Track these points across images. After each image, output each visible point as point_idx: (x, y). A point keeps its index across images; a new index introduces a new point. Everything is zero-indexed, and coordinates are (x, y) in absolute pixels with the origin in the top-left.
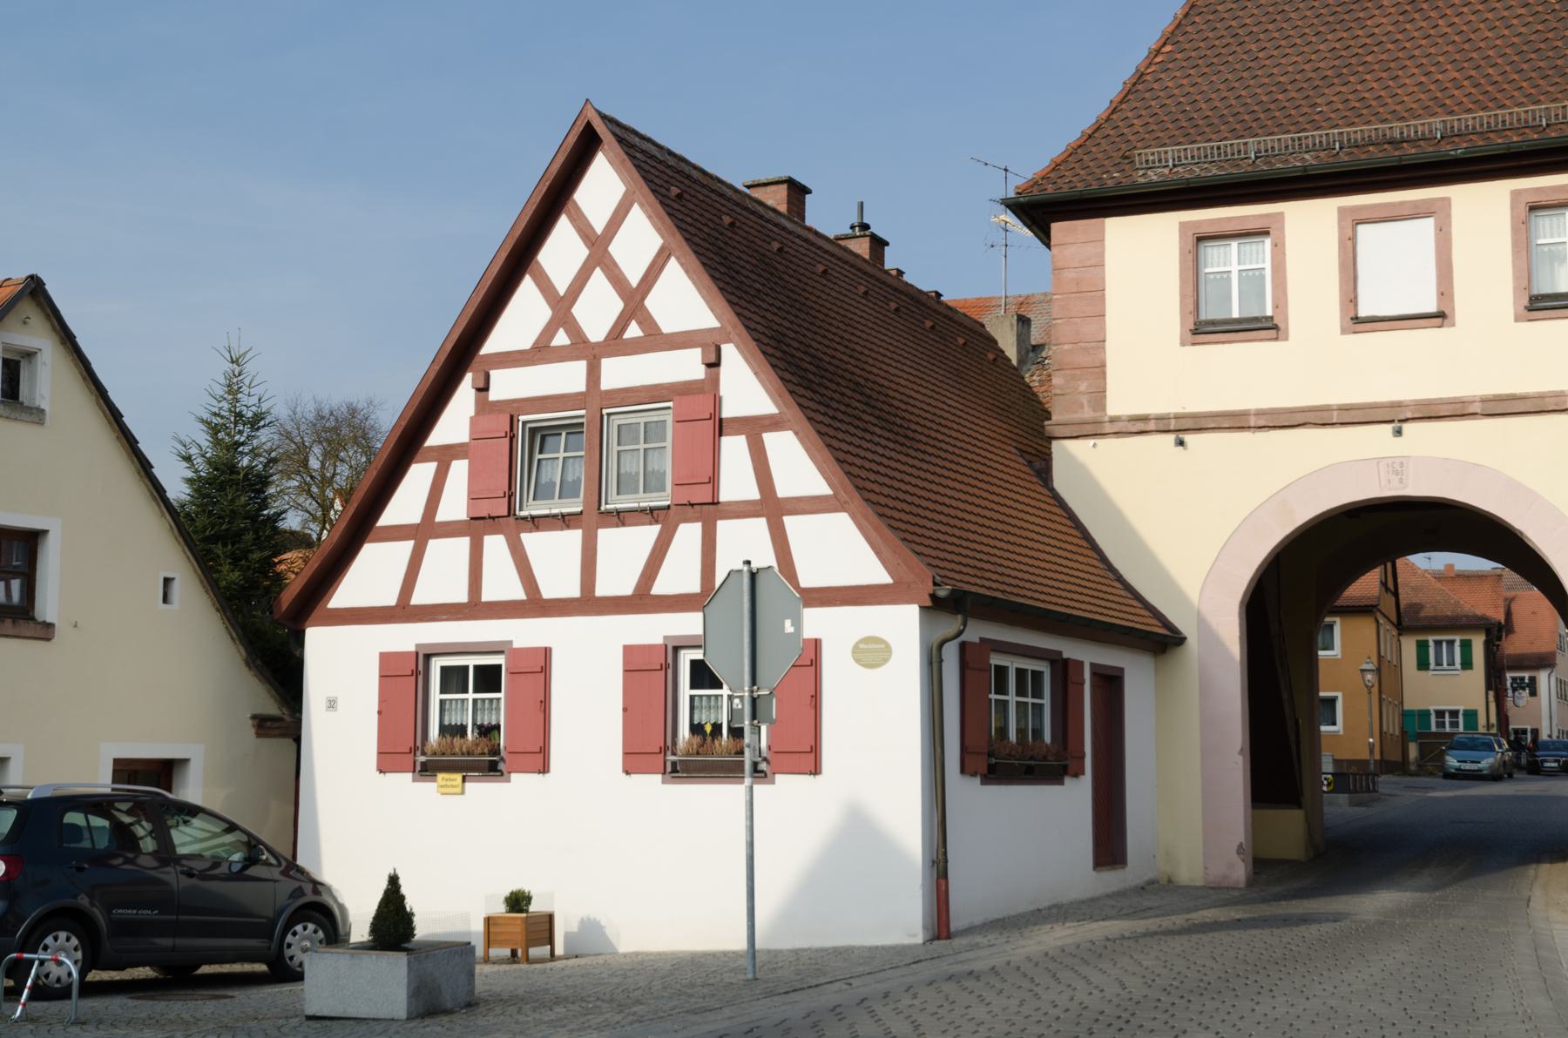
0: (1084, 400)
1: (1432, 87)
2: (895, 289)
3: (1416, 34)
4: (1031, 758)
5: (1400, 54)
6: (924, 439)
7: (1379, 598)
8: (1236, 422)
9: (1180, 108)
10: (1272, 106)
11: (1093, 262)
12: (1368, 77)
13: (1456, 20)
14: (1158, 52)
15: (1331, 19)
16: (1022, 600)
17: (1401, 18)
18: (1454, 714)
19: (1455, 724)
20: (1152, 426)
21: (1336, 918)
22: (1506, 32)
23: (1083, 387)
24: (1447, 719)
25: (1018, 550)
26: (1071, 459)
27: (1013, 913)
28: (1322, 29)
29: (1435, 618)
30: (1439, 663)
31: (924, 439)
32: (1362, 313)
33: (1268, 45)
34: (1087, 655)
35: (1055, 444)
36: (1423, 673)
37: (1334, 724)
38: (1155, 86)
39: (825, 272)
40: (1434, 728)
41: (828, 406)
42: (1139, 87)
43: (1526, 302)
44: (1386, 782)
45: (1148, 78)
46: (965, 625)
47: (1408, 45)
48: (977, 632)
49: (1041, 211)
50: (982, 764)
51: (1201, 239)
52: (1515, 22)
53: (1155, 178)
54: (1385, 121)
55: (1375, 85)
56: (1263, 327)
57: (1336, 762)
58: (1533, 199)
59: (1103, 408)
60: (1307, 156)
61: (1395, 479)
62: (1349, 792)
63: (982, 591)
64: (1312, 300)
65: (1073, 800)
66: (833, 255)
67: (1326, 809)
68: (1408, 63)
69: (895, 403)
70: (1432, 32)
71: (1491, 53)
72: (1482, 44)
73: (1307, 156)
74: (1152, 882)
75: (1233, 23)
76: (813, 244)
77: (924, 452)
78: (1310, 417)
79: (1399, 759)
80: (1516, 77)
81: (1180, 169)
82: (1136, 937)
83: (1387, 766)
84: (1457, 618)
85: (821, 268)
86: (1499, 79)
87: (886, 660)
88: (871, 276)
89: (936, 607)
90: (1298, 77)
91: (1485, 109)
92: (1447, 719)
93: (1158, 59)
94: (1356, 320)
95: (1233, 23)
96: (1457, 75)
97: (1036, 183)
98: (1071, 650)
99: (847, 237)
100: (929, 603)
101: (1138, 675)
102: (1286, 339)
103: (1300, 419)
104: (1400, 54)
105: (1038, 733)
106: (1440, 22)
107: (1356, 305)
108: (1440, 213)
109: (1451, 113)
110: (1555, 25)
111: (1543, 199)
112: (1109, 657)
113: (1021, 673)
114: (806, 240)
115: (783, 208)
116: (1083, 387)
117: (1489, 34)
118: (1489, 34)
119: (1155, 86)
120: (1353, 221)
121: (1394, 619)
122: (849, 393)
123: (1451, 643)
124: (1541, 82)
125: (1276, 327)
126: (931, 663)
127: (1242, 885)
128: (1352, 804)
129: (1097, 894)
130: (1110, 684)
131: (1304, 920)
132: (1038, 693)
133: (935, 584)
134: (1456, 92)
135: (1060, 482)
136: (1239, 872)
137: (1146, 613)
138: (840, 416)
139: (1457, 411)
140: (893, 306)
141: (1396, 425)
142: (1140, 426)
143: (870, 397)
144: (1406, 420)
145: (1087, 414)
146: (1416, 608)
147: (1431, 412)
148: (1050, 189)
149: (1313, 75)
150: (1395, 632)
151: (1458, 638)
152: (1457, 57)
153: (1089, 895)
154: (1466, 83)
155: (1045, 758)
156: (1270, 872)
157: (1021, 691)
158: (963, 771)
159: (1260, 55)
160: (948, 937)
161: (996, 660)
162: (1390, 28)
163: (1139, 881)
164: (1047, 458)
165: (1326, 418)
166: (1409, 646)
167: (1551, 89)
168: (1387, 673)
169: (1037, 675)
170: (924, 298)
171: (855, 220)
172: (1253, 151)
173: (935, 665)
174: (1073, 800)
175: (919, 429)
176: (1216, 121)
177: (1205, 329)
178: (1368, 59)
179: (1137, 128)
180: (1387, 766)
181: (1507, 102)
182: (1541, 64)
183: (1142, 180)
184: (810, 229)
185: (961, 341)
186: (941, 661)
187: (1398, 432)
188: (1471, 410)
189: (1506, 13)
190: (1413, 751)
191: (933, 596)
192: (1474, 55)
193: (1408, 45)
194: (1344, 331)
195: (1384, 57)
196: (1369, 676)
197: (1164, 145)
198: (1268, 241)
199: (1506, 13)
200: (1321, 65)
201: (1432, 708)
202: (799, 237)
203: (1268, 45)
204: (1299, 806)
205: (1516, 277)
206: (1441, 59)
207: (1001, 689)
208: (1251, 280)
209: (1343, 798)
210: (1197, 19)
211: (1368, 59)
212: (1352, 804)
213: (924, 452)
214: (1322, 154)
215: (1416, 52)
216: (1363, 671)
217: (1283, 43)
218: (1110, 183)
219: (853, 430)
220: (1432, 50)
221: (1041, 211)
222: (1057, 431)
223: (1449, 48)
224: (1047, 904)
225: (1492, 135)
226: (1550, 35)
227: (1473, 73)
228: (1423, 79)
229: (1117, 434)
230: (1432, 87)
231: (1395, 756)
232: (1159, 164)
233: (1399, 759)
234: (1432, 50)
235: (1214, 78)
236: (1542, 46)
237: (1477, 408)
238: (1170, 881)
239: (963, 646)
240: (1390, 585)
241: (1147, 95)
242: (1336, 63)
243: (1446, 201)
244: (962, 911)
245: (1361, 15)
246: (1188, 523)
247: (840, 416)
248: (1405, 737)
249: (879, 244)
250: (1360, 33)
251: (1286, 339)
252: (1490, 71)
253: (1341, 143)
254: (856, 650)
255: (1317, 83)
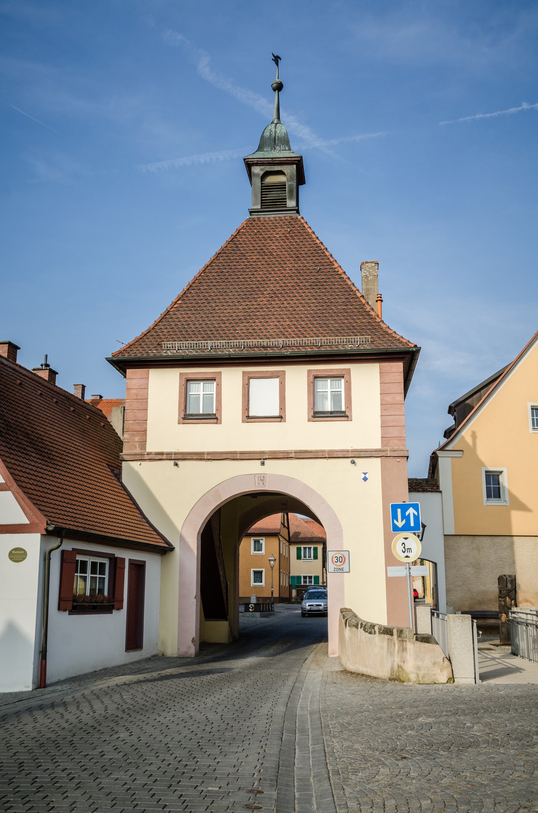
0: (137, 445)
1: (280, 327)
2: (58, 393)
3: (276, 306)
4: (96, 602)
5: (269, 313)
6: (58, 459)
7: (280, 529)
8: (199, 457)
9: (183, 326)
10: (219, 329)
11: (143, 387)
12: (257, 321)
13: (291, 302)
14: (176, 303)
15: (244, 297)
16: (93, 532)
17: (270, 299)
18: (310, 577)
19: (310, 582)
20: (164, 457)
21: (222, 671)
22: (308, 308)
23: (137, 439)
24: (308, 580)
25: (97, 509)
26: (132, 469)
27: (81, 673)
28: (241, 300)
29: (304, 538)
30: (305, 557)
31: (58, 459)
32: (251, 415)
33: (219, 304)
34: (127, 556)
35: (123, 463)
36: (299, 560)
37: (261, 582)
38: (174, 316)
39: (20, 384)
40: (302, 584)
41: (8, 443)
42: (167, 316)
43: (312, 414)
44: (278, 607)
45: (171, 313)
46: (61, 542)
47: (272, 310)
48: (69, 545)
49: (122, 364)
50: (70, 605)
51: (316, 377)
52: (312, 305)
53: (170, 354)
54: (262, 338)
55: (259, 324)
56: (213, 418)
57: (258, 598)
58: (316, 374)
59: (145, 449)
60: (231, 350)
61: (261, 483)
62: (260, 611)
63: (72, 527)
64: (231, 408)
65: (117, 621)
66: (27, 377)
67: (240, 620)
68: (272, 317)
69: (46, 442)
70: (282, 306)
71: (302, 316)
72: (299, 312)
73: (231, 350)
74: (154, 656)
75: (206, 294)
76: (17, 371)
77: (57, 465)
78: (229, 456)
79: (288, 597)
80: (311, 326)
81: (180, 351)
82: (139, 682)
83: (281, 600)
84: (313, 538)
85: (19, 382)
86: (305, 326)
87: (24, 559)
88: (46, 387)
89: (48, 534)
90: (230, 318)
91: (299, 337)
92: (308, 580)
93: (176, 306)
94: (248, 417)
95: (206, 294)
96: (290, 323)
97: (121, 352)
98: (119, 553)
99: (38, 369)
100: (45, 533)
101: (152, 565)
102: (221, 423)
103: (225, 456)
104: (269, 313)
105: (101, 591)
106: (285, 302)
107: (248, 411)
108: (281, 376)
109: (287, 338)
110: (326, 307)
111: (319, 374)
112: (138, 556)
113: (94, 564)
114: (14, 369)
115: (47, 379)
116: (137, 439)
117: (302, 309)
118: (302, 309)
119: (174, 316)
120: (248, 378)
121: (287, 538)
122: (21, 437)
123: (310, 548)
124: (320, 329)
125: (217, 418)
126: (45, 560)
127: (193, 656)
128: (261, 616)
129: (127, 662)
130: (138, 568)
131: (208, 672)
132: (102, 572)
133: (47, 524)
134: (289, 330)
135: (125, 480)
136: (192, 650)
137: (158, 537)
138: (14, 447)
139: (285, 456)
140: (55, 400)
141: (262, 460)
142: (160, 457)
143: (33, 439)
144: (266, 459)
145: (138, 451)
146: (297, 534)
147: (276, 456)
148: (127, 355)
149: (236, 318)
150: (287, 544)
151: (312, 546)
152: (290, 316)
153: (122, 663)
154: (293, 327)
155: (102, 602)
156: (208, 649)
157: (93, 571)
158: (59, 609)
159: (216, 308)
160: (45, 687)
161: (79, 558)
162: (266, 302)
163: (148, 656)
164: (120, 468)
165: (234, 456)
166: (293, 549)
167: (323, 332)
168: (284, 562)
169: (102, 565)
170: (72, 398)
171: (43, 362)
172: (210, 346)
173: (47, 561)
174: (117, 621)
175: (56, 454)
176: (197, 333)
177: (187, 417)
178: (257, 313)
179: (165, 333)
180: (281, 600)
181: (307, 336)
182: (320, 322)
183: (164, 354)
184: (17, 365)
185: (88, 417)
186: (50, 559)
187: (263, 464)
188: (291, 456)
189: (309, 301)
190: (294, 593)
191: (46, 530)
192: (296, 316)
193: (272, 310)
194: (243, 422)
195: (263, 313)
196: (272, 563)
197: (206, 340)
198: (343, 380)
199: (309, 301)
200: (239, 314)
201: (302, 575)
202: (10, 367)
203: (219, 304)
204: (227, 620)
205: (309, 404)
206: (284, 316)
207: (83, 570)
208: (208, 398)
209: (258, 614)
210: (192, 291)
211: (257, 313)
212: (261, 616)
213: (57, 465)
214: (237, 350)
215: (275, 313)
216: (269, 560)
217: (225, 304)
218: (152, 355)
219: (20, 454)
220: (281, 313)
221: (122, 364)
222: (126, 458)
223: (287, 312)
224: (100, 668)
225: (301, 348)
226: (324, 311)
227: (296, 323)
228: (277, 323)
229: (150, 460)
230: (280, 327)
231: (286, 595)
232: (172, 348)
233: (288, 597)
234: (281, 313)
235: (197, 316)
236: (321, 315)
237: (293, 455)
238: (163, 655)
239: (63, 552)
240: (286, 524)
241: (170, 320)
242: (245, 314)
243: (284, 372)
244: (52, 675)
245: (255, 296)
246: (176, 498)
247: (14, 447)
248: (291, 587)
249: (53, 374)
250: (255, 303)
251: (221, 423)
252: (302, 323)
253: (244, 346)
254: (11, 554)
255: (237, 321)
